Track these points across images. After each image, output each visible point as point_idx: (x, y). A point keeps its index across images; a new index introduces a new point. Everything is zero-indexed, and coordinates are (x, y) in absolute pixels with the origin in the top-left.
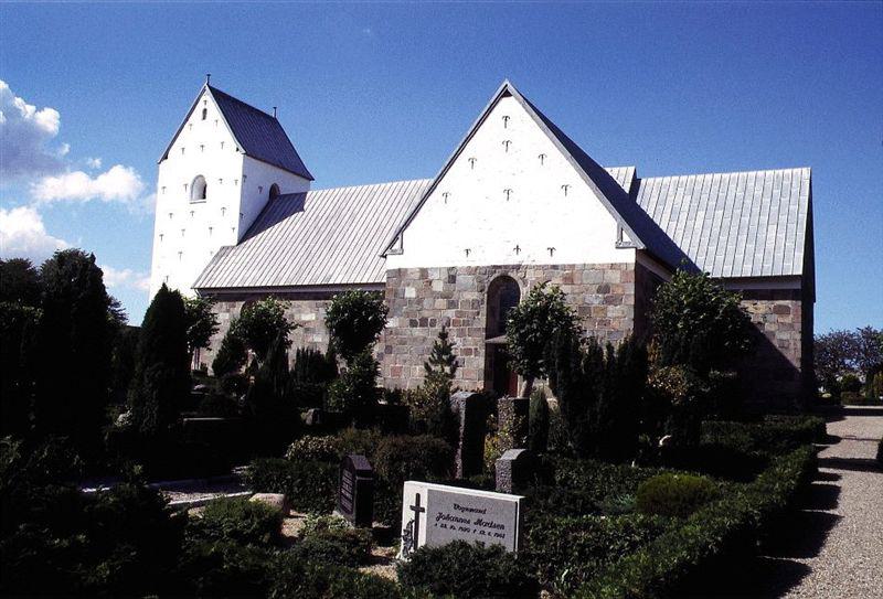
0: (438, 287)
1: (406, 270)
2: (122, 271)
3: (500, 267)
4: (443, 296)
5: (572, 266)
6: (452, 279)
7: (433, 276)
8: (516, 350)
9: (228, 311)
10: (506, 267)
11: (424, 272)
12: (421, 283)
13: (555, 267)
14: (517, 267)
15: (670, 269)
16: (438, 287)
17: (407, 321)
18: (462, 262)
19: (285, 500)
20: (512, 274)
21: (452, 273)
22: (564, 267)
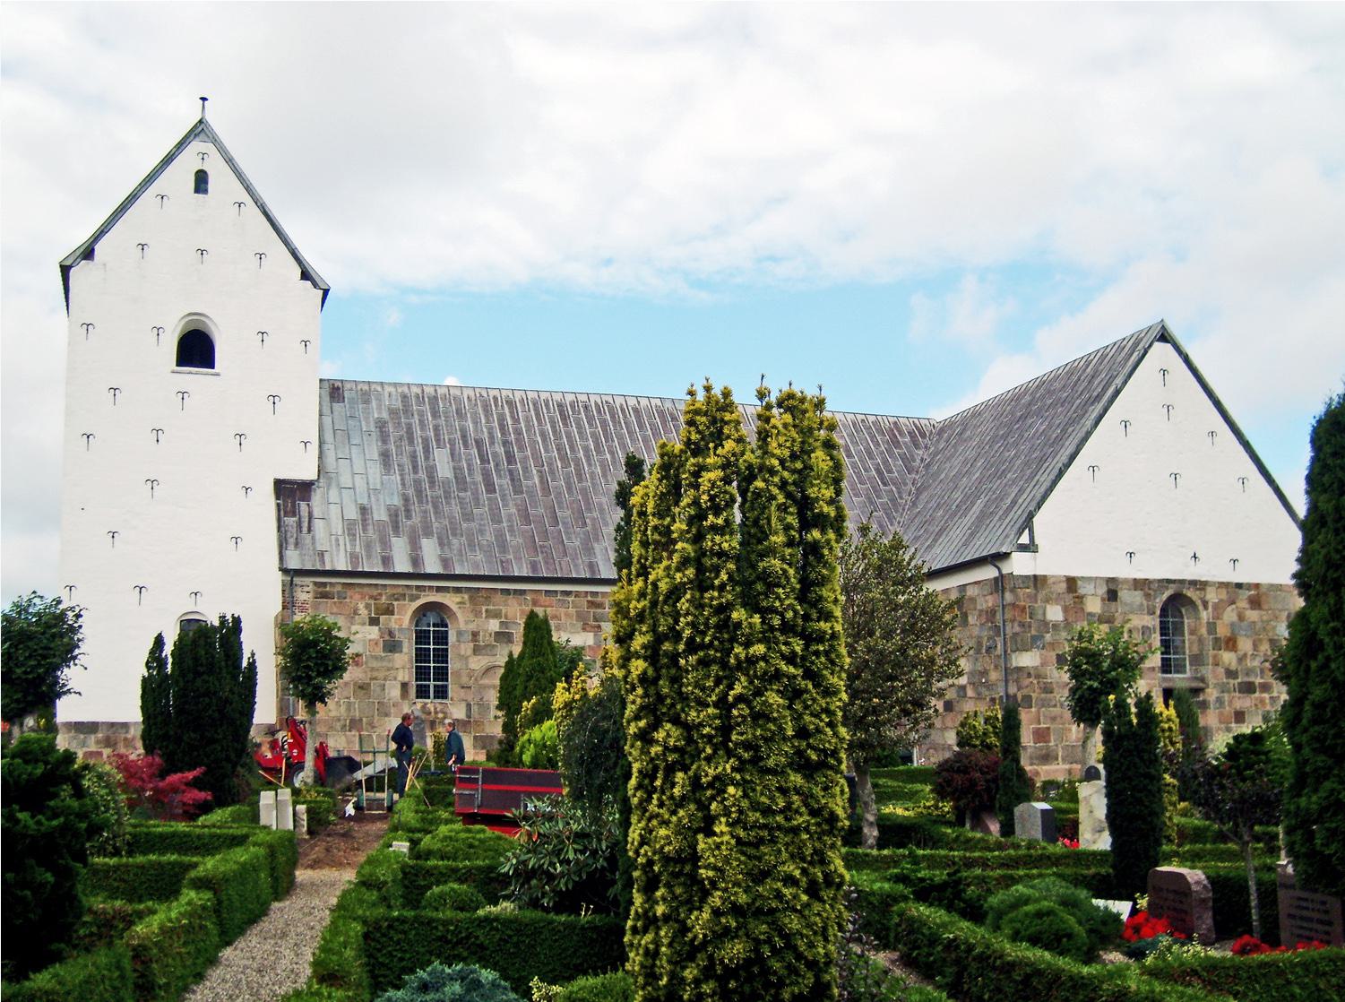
0: (1094, 606)
1: (1045, 576)
2: (1289, 627)
3: (1169, 581)
4: (1101, 620)
5: (1257, 586)
6: (1112, 595)
7: (1084, 589)
8: (477, 992)
9: (374, 622)
10: (1182, 582)
11: (1072, 583)
12: (1069, 599)
13: (1239, 586)
14: (1193, 583)
15: (1270, 967)
16: (1094, 606)
17: (1052, 656)
18: (1126, 571)
19: (1201, 748)
20: (1190, 593)
21: (1112, 587)
22: (1250, 586)
